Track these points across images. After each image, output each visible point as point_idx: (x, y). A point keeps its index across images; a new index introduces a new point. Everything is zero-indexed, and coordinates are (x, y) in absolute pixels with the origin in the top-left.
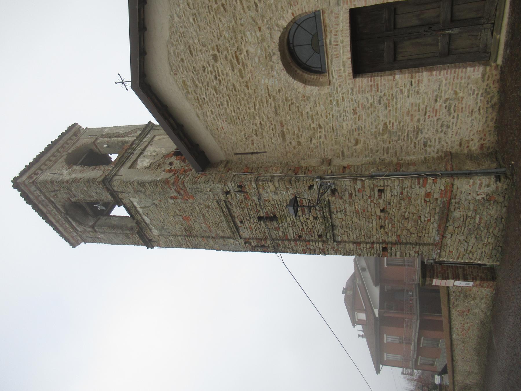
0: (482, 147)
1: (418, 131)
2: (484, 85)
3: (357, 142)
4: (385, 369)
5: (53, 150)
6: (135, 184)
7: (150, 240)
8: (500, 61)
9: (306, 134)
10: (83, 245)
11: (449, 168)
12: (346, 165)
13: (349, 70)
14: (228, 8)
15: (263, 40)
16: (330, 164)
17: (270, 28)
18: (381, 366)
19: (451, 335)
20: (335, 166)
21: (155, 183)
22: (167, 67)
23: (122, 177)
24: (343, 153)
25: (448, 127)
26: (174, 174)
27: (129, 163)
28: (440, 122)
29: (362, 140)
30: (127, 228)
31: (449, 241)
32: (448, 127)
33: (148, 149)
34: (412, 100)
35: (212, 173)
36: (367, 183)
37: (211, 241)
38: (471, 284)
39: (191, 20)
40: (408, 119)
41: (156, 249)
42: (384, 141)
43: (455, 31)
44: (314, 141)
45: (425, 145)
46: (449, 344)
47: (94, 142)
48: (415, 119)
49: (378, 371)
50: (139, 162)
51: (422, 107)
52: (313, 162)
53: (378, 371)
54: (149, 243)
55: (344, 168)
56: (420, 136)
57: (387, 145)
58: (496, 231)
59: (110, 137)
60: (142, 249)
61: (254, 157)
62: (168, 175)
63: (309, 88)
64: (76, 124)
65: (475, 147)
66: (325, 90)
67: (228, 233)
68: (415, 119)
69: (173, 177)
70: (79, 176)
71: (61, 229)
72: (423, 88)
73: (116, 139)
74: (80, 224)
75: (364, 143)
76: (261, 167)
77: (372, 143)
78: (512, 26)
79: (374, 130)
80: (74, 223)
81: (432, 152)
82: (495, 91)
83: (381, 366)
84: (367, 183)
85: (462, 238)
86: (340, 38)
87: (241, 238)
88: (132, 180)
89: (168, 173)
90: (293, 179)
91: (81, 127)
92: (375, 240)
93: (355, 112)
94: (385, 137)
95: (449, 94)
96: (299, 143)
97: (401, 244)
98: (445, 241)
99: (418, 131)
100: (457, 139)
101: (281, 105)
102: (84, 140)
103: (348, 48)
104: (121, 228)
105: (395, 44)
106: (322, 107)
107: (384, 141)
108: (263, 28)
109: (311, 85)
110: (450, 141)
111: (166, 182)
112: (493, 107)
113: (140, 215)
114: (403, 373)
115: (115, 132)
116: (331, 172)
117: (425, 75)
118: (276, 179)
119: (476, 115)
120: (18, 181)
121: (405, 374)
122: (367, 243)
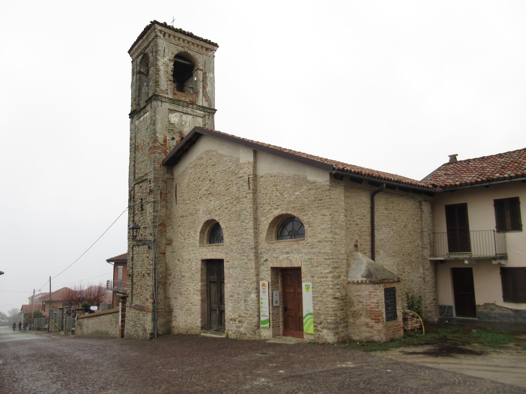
0: (174, 327)
1: (181, 294)
2: (195, 327)
3: (179, 260)
4: (111, 266)
5: (189, 39)
6: (154, 118)
7: (133, 117)
8: (202, 334)
9: (182, 231)
10: (129, 59)
11: (160, 310)
12: (166, 254)
13: (206, 258)
14: (227, 192)
15: (216, 210)
16: (167, 244)
17: (219, 215)
18: (113, 263)
19: (103, 314)
20: (166, 248)
21: (155, 132)
22: (208, 149)
23: (159, 108)
24: (175, 252)
25: (182, 310)
26: (162, 145)
27: (172, 107)
28: (183, 306)
29: (179, 263)
30: (139, 101)
31: (132, 311)
32: (182, 310)
33: (189, 116)
34: (192, 291)
35: (162, 171)
36: (152, 267)
37: (133, 163)
38: (120, 324)
39: (224, 168)
40: (185, 289)
41: (129, 120)
42: (178, 275)
43: (218, 312)
44: (180, 235)
45: (176, 298)
46: (100, 314)
47: (198, 69)
48: (185, 293)
49: (109, 261)
50: (175, 114)
51: (189, 296)
52: (169, 235)
53: (109, 261)
54: (132, 115)
55: (164, 254)
56: (179, 295)
57: (176, 277)
58: (135, 335)
59: (203, 81)
60: (129, 110)
61: (175, 197)
62: (161, 141)
63: (198, 234)
64: (218, 47)
65: (174, 324)
66: (198, 244)
67: (137, 177)
68: (185, 293)
69: (159, 145)
70: (162, 73)
71: (136, 46)
72: (196, 296)
73: (202, 86)
74: (141, 63)
75: (178, 265)
76: (167, 202)
77: (178, 269)
78: (215, 339)
79: (183, 270)
80: (140, 57)
81: (173, 302)
82: (192, 333)
83: (113, 263)
84: (152, 267)
85: (133, 318)
86: (215, 253)
87: (134, 185)
88: (157, 116)
89: (163, 140)
90: (155, 224)
91: (215, 51)
92: (134, 270)
93: (189, 260)
94: (180, 276)
95: (193, 310)
96: (179, 226)
97: (132, 285)
98: (132, 309)
99: (181, 294)
100: (177, 315)
101: (194, 217)
102: (200, 59)
103: (211, 258)
104: (138, 96)
105: (216, 282)
106: (192, 241)
107: (178, 275)
108: (219, 211)
109: (200, 236)
110: (177, 312)
111: (156, 141)
112: (187, 332)
113: (143, 115)
114: (108, 281)
115: (208, 83)
116: (160, 246)
117: (199, 298)
118: (156, 214)
119: (185, 324)
120: (156, 25)
121: (107, 284)
122: (132, 265)
